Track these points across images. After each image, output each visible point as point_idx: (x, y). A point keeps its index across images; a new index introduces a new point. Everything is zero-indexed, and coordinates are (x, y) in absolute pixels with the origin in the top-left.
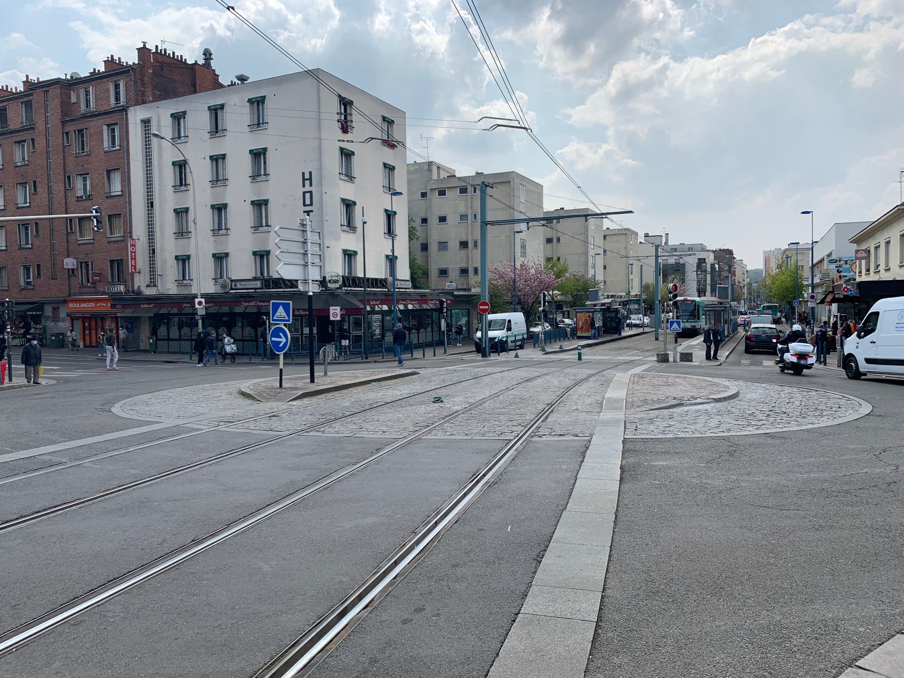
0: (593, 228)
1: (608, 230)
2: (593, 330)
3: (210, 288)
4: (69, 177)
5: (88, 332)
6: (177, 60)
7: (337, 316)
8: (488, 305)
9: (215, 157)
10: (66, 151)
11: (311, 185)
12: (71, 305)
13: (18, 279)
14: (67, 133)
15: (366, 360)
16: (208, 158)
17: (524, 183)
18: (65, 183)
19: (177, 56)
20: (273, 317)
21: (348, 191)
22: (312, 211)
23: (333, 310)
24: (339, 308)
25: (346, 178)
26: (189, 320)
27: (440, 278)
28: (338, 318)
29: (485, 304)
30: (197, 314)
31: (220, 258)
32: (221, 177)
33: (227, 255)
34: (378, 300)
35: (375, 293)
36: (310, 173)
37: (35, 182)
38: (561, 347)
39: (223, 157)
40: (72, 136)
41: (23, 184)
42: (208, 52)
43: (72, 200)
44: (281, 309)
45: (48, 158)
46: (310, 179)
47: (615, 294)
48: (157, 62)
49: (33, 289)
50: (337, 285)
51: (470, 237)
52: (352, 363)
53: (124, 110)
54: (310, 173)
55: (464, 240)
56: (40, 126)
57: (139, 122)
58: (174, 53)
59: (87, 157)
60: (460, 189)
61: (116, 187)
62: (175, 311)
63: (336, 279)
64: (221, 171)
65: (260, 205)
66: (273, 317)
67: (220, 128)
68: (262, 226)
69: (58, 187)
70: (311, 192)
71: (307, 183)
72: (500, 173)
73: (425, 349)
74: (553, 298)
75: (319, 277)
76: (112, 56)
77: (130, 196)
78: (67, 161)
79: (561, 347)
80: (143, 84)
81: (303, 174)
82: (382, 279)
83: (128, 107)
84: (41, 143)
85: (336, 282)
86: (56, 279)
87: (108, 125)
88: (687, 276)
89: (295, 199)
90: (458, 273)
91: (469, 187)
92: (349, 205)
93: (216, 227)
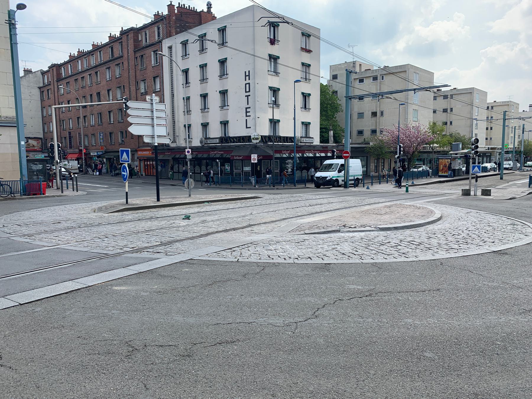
0: (477, 101)
1: (495, 103)
2: (450, 171)
3: (196, 143)
4: (138, 82)
5: (146, 167)
6: (191, 10)
7: (255, 160)
8: (349, 153)
9: (202, 66)
10: (136, 67)
11: (249, 79)
12: (139, 153)
13: (118, 139)
14: (136, 58)
15: (274, 188)
16: (198, 66)
17: (417, 72)
18: (136, 86)
19: (192, 8)
20: (121, 159)
21: (274, 82)
22: (250, 95)
23: (253, 156)
24: (256, 155)
25: (274, 74)
26: (182, 161)
27: (358, 137)
28: (256, 161)
29: (347, 153)
30: (186, 158)
31: (205, 126)
32: (205, 78)
33: (208, 123)
34: (289, 150)
35: (287, 146)
36: (249, 71)
37: (124, 86)
38: (413, 183)
39: (206, 65)
40: (139, 59)
41: (119, 87)
42: (209, 3)
43: (139, 95)
44: (125, 154)
45: (129, 73)
46: (249, 76)
47: (495, 147)
48: (179, 12)
49: (124, 144)
50: (258, 141)
51: (378, 109)
52: (263, 189)
53: (160, 42)
54: (249, 71)
55: (375, 111)
56: (126, 56)
57: (167, 48)
58: (189, 6)
59: (145, 70)
60: (373, 78)
61: (158, 87)
62: (205, 156)
63: (257, 137)
64: (205, 74)
65: (224, 93)
66: (121, 159)
67: (204, 48)
68: (225, 106)
69: (133, 88)
70: (249, 84)
71: (247, 77)
72: (399, 66)
73: (306, 183)
74: (433, 150)
75: (166, 134)
76: (158, 12)
77: (163, 91)
78: (137, 73)
79: (413, 183)
80: (170, 27)
81: (245, 72)
82: (291, 137)
83: (162, 40)
84: (126, 64)
85: (257, 139)
86: (133, 138)
87: (154, 52)
88: (417, 128)
89: (241, 88)
90: (369, 133)
91: (379, 76)
92: (275, 91)
93: (203, 108)
